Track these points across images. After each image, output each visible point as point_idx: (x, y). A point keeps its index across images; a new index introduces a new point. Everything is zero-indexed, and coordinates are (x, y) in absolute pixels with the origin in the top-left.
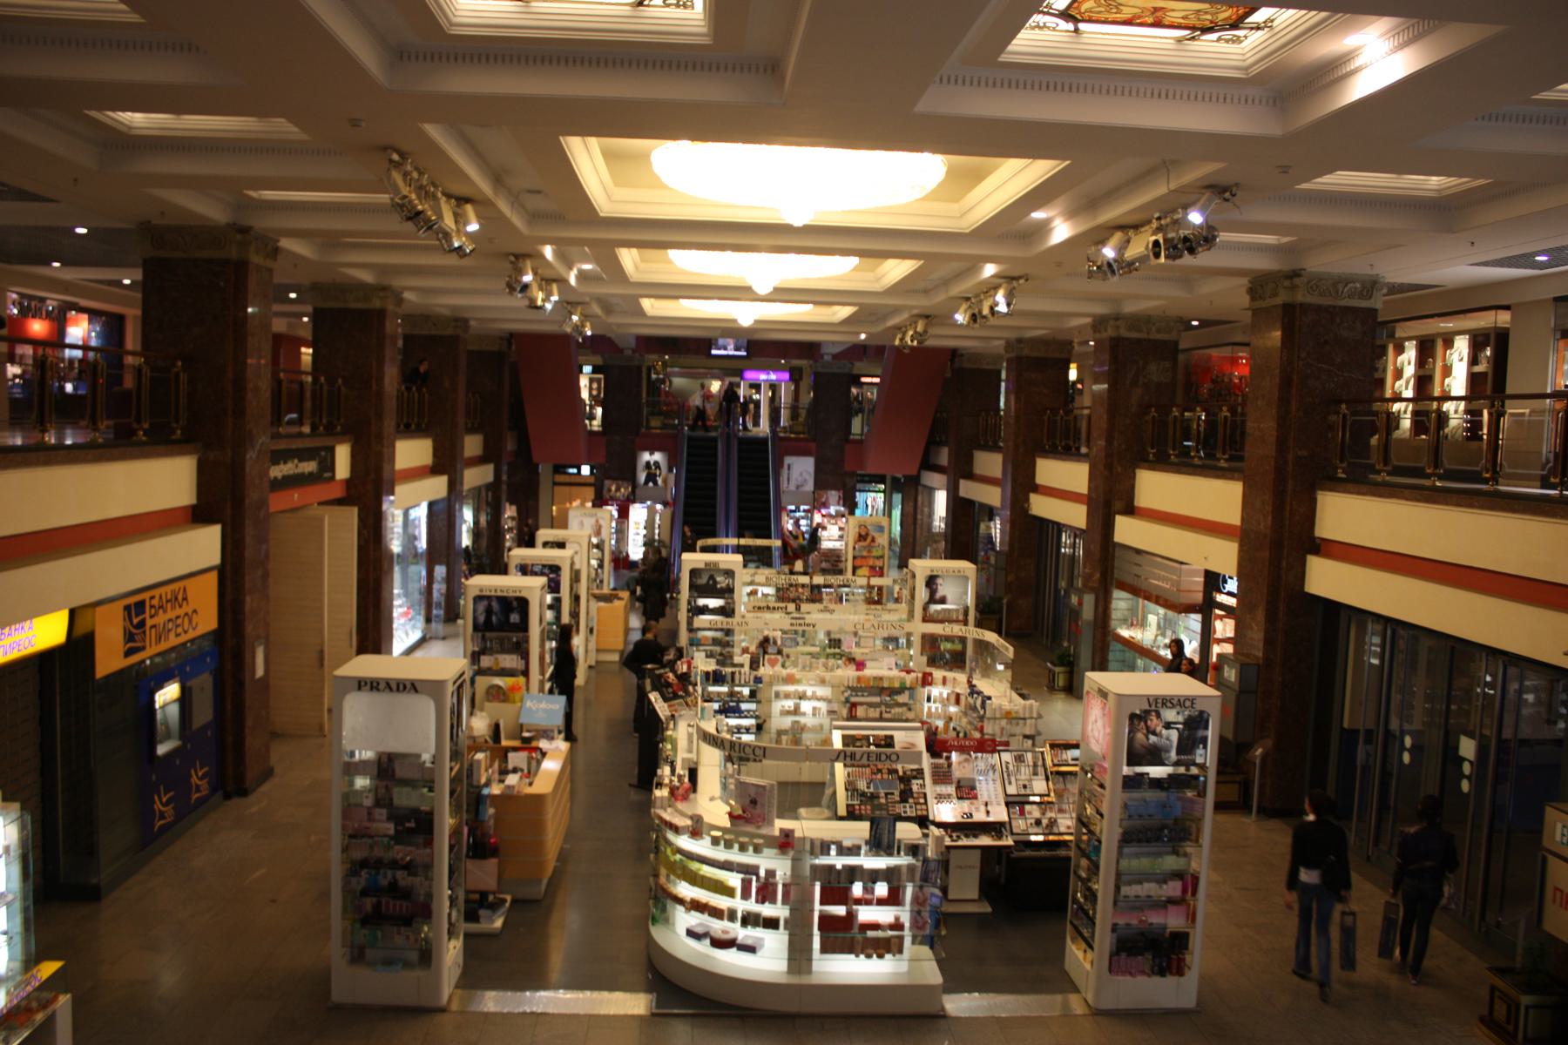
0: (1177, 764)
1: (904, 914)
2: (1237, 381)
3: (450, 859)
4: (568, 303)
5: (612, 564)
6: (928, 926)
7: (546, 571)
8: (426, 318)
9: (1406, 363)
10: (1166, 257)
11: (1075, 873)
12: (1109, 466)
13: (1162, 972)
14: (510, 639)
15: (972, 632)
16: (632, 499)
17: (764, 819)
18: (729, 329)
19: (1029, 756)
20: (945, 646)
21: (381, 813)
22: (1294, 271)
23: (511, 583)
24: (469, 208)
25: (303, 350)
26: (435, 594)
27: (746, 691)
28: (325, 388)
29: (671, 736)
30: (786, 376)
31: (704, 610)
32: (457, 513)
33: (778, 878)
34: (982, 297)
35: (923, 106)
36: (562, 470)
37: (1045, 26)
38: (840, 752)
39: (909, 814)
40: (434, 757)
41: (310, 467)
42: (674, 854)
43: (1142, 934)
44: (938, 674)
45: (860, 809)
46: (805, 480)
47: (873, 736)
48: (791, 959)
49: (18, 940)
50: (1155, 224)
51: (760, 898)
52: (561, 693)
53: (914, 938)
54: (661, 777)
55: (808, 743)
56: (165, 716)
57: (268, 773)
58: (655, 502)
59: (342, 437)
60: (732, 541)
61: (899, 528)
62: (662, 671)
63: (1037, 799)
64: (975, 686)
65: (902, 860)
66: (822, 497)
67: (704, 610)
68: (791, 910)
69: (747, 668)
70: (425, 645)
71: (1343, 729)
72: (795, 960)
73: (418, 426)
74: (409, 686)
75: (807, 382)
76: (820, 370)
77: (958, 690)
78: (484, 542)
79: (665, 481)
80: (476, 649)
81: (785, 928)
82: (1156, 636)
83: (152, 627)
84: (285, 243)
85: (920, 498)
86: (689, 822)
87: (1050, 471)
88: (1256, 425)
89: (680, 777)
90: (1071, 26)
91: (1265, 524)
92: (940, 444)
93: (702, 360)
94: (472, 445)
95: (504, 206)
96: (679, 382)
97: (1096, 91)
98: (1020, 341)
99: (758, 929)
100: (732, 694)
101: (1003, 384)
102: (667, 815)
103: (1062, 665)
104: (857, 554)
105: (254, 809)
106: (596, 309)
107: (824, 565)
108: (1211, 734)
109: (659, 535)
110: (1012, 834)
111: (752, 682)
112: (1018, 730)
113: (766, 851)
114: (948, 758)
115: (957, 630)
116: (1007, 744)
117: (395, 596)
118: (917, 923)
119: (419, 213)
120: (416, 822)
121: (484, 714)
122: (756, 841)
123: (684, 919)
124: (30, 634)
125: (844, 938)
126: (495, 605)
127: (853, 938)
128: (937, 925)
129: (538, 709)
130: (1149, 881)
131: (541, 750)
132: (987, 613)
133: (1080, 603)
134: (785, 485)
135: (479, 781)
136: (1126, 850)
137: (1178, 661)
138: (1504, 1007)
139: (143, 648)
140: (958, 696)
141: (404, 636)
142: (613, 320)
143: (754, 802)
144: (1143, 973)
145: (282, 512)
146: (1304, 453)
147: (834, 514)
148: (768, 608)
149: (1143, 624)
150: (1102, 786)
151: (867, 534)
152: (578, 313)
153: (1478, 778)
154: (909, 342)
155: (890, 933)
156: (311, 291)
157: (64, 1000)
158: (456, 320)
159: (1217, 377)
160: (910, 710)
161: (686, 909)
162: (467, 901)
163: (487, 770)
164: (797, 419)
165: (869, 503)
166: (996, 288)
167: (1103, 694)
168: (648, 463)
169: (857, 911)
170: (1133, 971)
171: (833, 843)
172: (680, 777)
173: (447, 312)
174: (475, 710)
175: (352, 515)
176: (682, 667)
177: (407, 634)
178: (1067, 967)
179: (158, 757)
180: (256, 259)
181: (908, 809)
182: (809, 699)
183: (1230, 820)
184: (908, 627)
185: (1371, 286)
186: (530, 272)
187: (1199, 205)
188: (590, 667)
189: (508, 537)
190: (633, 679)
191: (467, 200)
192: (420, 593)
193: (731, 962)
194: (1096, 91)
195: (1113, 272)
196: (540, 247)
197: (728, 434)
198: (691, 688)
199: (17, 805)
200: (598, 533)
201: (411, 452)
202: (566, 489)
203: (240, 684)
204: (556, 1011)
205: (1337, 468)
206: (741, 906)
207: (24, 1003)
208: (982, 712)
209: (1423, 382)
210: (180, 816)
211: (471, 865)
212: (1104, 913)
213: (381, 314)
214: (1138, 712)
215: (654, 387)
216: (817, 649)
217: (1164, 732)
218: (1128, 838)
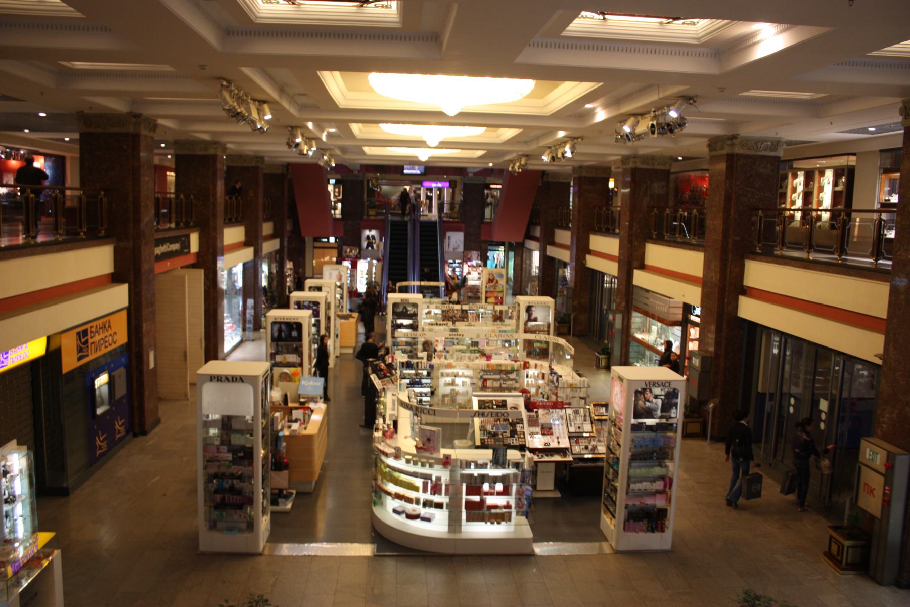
0: (661, 417)
1: (512, 500)
2: (705, 190)
3: (263, 472)
4: (321, 149)
5: (348, 295)
6: (525, 507)
7: (312, 305)
8: (240, 157)
9: (798, 184)
10: (658, 133)
11: (606, 477)
12: (631, 242)
13: (653, 530)
14: (292, 345)
15: (552, 339)
16: (359, 257)
17: (434, 449)
18: (414, 162)
19: (582, 411)
20: (537, 345)
21: (225, 448)
22: (733, 135)
23: (290, 314)
24: (266, 107)
25: (168, 173)
26: (248, 316)
27: (425, 373)
28: (184, 201)
29: (383, 401)
30: (447, 184)
31: (401, 326)
32: (259, 266)
33: (442, 481)
34: (558, 147)
35: (518, 60)
36: (318, 240)
37: (586, 17)
38: (476, 412)
39: (515, 443)
40: (253, 417)
41: (176, 247)
42: (385, 468)
43: (642, 509)
44: (532, 362)
45: (488, 441)
46: (459, 246)
47: (495, 400)
48: (450, 525)
49: (29, 520)
50: (652, 114)
51: (433, 492)
52: (321, 376)
53: (517, 514)
54: (377, 425)
55: (460, 402)
56: (100, 393)
57: (157, 422)
58: (372, 259)
59: (193, 228)
60: (417, 283)
61: (512, 272)
62: (377, 362)
63: (588, 435)
64: (553, 369)
65: (511, 471)
66: (468, 255)
67: (401, 326)
68: (450, 498)
69: (425, 360)
70: (242, 344)
71: (758, 392)
72: (452, 525)
73: (236, 219)
74: (238, 379)
75: (459, 187)
76: (467, 182)
77: (543, 372)
78: (275, 283)
79: (378, 247)
80: (273, 351)
81: (447, 508)
82: (656, 338)
83: (92, 343)
84: (160, 122)
85: (524, 255)
86: (393, 451)
87: (598, 242)
88: (711, 222)
89: (388, 426)
90: (601, 17)
91: (715, 277)
92: (536, 224)
93: (398, 176)
94: (267, 228)
95: (285, 104)
96: (385, 188)
97: (616, 50)
98: (581, 167)
99: (432, 509)
100: (417, 375)
101: (572, 188)
102: (381, 447)
103: (604, 354)
104: (488, 290)
105: (151, 442)
106: (338, 152)
107: (469, 294)
108: (680, 401)
109: (375, 278)
110: (572, 454)
111: (428, 368)
112: (577, 394)
113: (436, 467)
114: (537, 412)
115: (542, 337)
116: (569, 404)
117: (225, 318)
118: (518, 506)
119: (238, 114)
120: (244, 453)
121: (279, 389)
122: (430, 461)
123: (391, 504)
124: (26, 350)
125: (479, 514)
126: (283, 327)
127: (484, 514)
128: (530, 505)
129: (308, 386)
130: (646, 481)
131: (310, 408)
132: (563, 326)
133: (614, 319)
134: (447, 248)
135: (277, 428)
136: (633, 465)
137: (668, 353)
138: (836, 546)
139: (88, 355)
140: (543, 375)
141: (230, 340)
142: (347, 157)
143: (429, 440)
144: (642, 531)
145: (161, 273)
146: (738, 238)
147: (475, 265)
148: (437, 324)
149: (649, 331)
150: (620, 429)
151: (494, 279)
152: (327, 155)
153: (828, 422)
154: (517, 170)
155: (504, 510)
156: (176, 144)
157: (57, 553)
158: (257, 157)
159: (693, 188)
160: (517, 382)
161: (392, 498)
162: (272, 494)
163: (281, 421)
164: (454, 210)
165: (496, 257)
166: (565, 143)
167: (621, 379)
168: (368, 237)
169: (486, 499)
170: (637, 530)
171: (473, 462)
172: (388, 426)
173: (252, 154)
174: (274, 387)
175: (200, 274)
176: (389, 360)
177: (232, 339)
178: (601, 527)
179: (97, 416)
180: (144, 132)
181: (515, 441)
182: (460, 377)
183: (692, 443)
184: (515, 336)
185: (776, 143)
186: (300, 136)
187: (677, 105)
188: (337, 357)
189: (288, 280)
190: (361, 363)
191: (264, 102)
192: (239, 315)
193: (417, 527)
194: (616, 50)
195: (629, 139)
196: (306, 123)
197: (414, 220)
198: (394, 372)
199: (25, 447)
200: (340, 279)
201: (233, 234)
202: (321, 250)
203: (140, 372)
204: (322, 555)
205: (756, 247)
206: (423, 496)
207: (37, 555)
208: (557, 384)
209: (808, 196)
210: (110, 448)
211: (273, 475)
212: (621, 498)
213: (214, 158)
214: (640, 389)
215: (371, 192)
216: (465, 347)
217: (654, 400)
218: (634, 458)
